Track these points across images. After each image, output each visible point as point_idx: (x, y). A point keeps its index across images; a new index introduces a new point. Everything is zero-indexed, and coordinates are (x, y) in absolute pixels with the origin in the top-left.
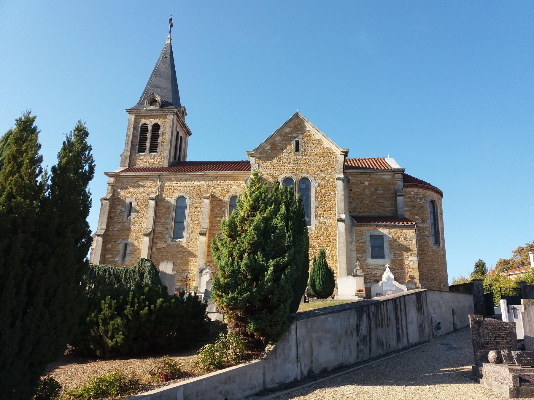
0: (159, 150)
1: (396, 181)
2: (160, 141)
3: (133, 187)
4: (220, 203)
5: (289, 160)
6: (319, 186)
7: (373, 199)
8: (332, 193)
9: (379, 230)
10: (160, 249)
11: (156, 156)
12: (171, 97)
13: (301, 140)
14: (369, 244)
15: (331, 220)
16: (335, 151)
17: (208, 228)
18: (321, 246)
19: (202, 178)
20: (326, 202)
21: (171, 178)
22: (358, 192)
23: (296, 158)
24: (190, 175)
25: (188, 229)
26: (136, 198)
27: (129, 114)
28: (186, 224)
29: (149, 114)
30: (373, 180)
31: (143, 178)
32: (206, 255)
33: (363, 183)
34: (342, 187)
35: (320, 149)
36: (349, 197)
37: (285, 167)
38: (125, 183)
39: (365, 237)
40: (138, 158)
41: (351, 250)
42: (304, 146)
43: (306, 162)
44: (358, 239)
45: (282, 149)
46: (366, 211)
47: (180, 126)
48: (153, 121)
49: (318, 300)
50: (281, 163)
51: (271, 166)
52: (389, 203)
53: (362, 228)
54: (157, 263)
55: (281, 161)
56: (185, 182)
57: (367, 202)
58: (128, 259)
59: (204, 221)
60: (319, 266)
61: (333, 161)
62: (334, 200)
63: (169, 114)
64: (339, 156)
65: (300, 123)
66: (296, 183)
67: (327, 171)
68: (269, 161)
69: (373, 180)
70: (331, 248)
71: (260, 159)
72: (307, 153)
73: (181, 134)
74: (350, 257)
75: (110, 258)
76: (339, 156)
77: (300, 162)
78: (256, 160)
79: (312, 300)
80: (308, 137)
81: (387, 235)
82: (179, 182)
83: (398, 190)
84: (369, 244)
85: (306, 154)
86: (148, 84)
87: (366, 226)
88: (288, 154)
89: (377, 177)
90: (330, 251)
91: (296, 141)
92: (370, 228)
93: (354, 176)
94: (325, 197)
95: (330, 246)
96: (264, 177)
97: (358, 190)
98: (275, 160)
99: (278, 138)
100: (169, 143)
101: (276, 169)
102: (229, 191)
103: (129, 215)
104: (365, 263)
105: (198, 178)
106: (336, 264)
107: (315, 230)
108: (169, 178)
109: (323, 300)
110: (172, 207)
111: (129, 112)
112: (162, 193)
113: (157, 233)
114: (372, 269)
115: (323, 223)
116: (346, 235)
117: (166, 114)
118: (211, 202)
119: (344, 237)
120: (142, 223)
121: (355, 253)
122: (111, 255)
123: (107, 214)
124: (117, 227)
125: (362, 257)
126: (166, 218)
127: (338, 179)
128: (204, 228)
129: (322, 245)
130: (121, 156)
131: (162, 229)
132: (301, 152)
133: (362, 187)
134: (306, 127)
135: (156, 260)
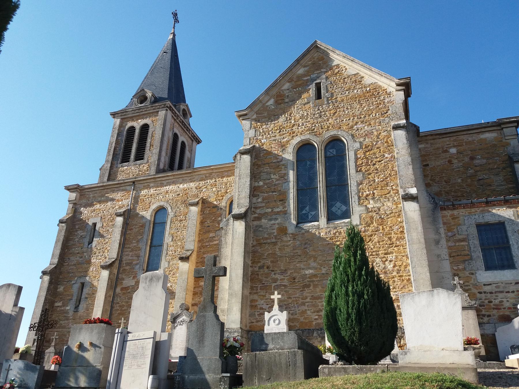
0: (146, 157)
1: (507, 141)
2: (148, 145)
3: (100, 202)
4: (215, 210)
5: (306, 114)
6: (361, 147)
7: (468, 175)
8: (386, 155)
9: (494, 211)
10: (126, 288)
11: (142, 164)
12: (166, 92)
13: (324, 81)
14: (475, 242)
15: (389, 204)
16: (386, 87)
17: (196, 250)
18: (374, 253)
19: (190, 178)
20: (377, 173)
21: (148, 184)
22: (439, 167)
23: (317, 109)
24: (174, 175)
25: (167, 254)
26: (101, 217)
27: (114, 118)
28: (165, 246)
29: (138, 114)
30: (464, 144)
31: (114, 189)
32: (191, 294)
33: (446, 151)
34: (405, 141)
35: (359, 89)
36: (425, 176)
37: (299, 126)
38: (90, 198)
39: (464, 228)
40: (120, 168)
41: (439, 256)
42: (330, 89)
43: (336, 113)
44: (450, 234)
45: (293, 101)
46: (459, 197)
47: (180, 128)
48: (142, 122)
49: (345, 371)
50: (293, 122)
51: (276, 128)
52: (501, 178)
53: (455, 212)
54: (121, 310)
55: (293, 118)
56: (167, 187)
57: (459, 181)
58: (83, 307)
59: (189, 240)
60: (346, 272)
61: (384, 102)
62: (392, 168)
63: (160, 109)
64: (395, 93)
65: (322, 57)
66: (320, 148)
67: (373, 121)
68: (272, 121)
69: (464, 144)
70: (397, 257)
71: (259, 121)
72: (336, 98)
73: (181, 139)
74: (437, 272)
75: (61, 307)
76: (395, 93)
77: (325, 114)
78: (251, 124)
79: (326, 371)
80: (336, 74)
81: (513, 221)
82: (160, 188)
83: (513, 154)
84: (477, 242)
85: (334, 101)
86: (142, 83)
87: (464, 208)
88: (304, 105)
89: (470, 139)
90: (393, 262)
91: (316, 84)
92: (473, 210)
93: (429, 142)
94: (374, 164)
95: (392, 253)
96: (265, 147)
97: (439, 163)
98: (282, 119)
99: (287, 86)
100: (159, 145)
101: (285, 132)
102: (228, 191)
103: (91, 242)
104: (472, 281)
105: (184, 178)
106: (410, 288)
107: (361, 224)
108: (146, 184)
109: (361, 370)
110: (147, 224)
111: (114, 115)
112: (136, 206)
113: (125, 265)
114: (491, 293)
115: (375, 211)
116: (424, 228)
117: (157, 110)
118: (202, 211)
119: (420, 228)
120: (106, 251)
121: (448, 262)
122: (61, 302)
123: (61, 242)
124: (74, 259)
125: (464, 269)
126: (138, 242)
127: (396, 127)
128: (188, 250)
129: (376, 251)
130: (100, 169)
131: (131, 258)
132: (325, 99)
133: (446, 158)
134: (332, 60)
135: (120, 306)
